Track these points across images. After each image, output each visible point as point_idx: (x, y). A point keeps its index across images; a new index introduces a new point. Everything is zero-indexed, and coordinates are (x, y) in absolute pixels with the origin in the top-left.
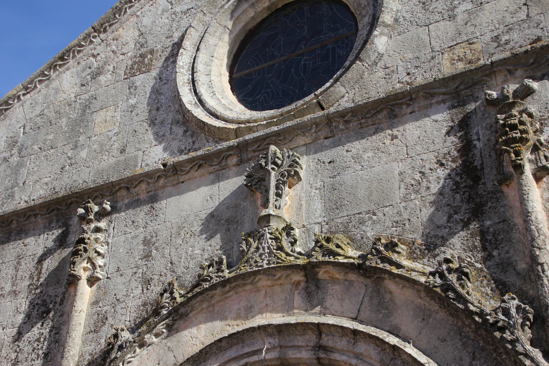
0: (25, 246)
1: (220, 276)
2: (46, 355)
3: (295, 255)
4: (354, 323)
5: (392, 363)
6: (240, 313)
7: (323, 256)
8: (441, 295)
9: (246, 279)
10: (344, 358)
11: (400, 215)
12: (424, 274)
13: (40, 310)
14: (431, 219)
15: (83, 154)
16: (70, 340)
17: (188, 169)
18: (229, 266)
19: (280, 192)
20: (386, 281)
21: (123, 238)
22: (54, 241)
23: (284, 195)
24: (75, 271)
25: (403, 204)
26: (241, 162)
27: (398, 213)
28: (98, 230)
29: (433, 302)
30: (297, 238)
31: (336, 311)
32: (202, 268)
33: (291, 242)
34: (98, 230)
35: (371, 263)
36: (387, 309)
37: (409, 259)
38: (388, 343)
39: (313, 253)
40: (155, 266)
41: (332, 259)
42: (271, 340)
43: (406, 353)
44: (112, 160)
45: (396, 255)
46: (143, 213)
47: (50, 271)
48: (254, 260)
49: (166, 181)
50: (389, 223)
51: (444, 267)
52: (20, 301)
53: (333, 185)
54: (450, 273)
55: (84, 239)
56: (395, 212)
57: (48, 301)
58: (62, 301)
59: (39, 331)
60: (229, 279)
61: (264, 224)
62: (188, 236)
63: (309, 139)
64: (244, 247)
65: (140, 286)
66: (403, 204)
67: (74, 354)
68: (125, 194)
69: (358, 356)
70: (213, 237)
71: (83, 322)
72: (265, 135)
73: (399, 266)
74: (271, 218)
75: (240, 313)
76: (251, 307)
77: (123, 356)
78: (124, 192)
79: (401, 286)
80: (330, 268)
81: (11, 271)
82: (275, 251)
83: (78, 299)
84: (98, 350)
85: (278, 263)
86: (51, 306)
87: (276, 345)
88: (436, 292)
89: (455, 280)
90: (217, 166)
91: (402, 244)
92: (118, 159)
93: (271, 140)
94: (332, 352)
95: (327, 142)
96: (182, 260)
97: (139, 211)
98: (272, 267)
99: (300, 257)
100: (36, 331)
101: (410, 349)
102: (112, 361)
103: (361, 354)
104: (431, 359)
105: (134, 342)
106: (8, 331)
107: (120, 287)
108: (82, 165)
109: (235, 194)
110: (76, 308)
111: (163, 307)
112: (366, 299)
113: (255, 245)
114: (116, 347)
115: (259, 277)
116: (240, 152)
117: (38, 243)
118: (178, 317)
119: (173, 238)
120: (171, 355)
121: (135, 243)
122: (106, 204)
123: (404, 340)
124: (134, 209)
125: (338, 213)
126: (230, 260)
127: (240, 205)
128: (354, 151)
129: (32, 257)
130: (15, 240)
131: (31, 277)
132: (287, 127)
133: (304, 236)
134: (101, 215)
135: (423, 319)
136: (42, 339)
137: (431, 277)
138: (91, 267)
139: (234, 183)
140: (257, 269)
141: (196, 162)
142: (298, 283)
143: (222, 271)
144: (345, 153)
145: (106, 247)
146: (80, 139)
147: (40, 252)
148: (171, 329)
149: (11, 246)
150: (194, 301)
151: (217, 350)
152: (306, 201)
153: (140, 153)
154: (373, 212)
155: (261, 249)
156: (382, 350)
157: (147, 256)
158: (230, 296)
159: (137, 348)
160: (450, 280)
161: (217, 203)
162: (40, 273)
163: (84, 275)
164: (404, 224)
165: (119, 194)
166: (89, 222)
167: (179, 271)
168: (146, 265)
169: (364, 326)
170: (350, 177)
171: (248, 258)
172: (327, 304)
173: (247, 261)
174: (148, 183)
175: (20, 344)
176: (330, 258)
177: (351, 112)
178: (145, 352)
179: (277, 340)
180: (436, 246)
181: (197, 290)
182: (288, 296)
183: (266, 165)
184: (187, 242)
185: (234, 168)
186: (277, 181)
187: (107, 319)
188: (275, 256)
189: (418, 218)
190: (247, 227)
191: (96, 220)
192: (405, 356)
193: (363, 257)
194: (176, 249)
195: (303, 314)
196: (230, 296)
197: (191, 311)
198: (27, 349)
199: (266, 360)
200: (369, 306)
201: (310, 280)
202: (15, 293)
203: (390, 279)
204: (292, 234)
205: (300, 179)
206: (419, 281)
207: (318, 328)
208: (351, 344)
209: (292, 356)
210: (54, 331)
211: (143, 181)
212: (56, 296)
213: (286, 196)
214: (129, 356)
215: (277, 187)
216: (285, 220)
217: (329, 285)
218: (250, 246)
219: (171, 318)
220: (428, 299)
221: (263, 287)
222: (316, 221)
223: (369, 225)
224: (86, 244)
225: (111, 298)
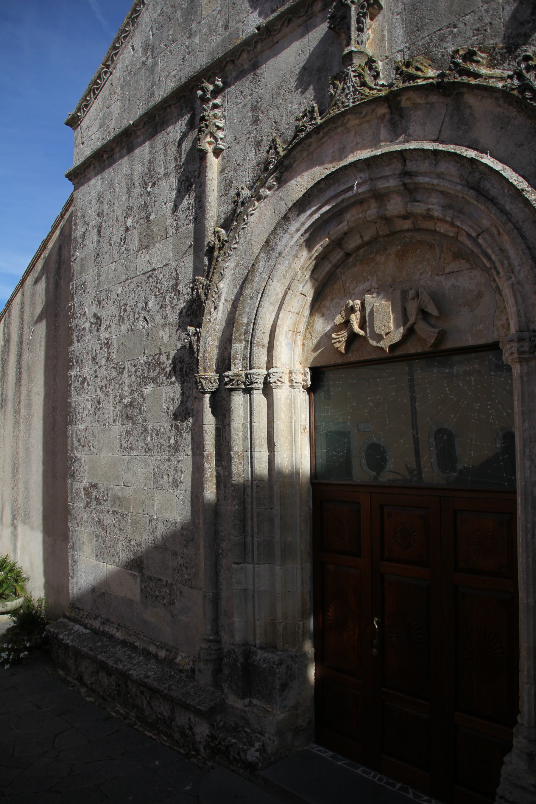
0: (168, 134)
2: (195, 219)
4: (434, 144)
5: (470, 176)
6: (335, 156)
7: (403, 83)
8: (518, 97)
10: (427, 180)
11: (481, 21)
12: (502, 79)
13: (186, 185)
14: (514, 16)
15: (197, 40)
16: (207, 205)
17: (279, 27)
18: (321, 114)
19: (362, 26)
20: (466, 96)
21: (235, 109)
22: (187, 125)
23: (365, 29)
24: (200, 146)
25: (485, 7)
27: (479, 19)
28: (215, 106)
29: (511, 108)
31: (419, 137)
32: (298, 120)
33: (373, 76)
34: (215, 106)
35: (449, 79)
36: (467, 125)
37: (490, 68)
38: (465, 157)
40: (263, 129)
41: (412, 84)
42: (362, 175)
43: (483, 163)
44: (219, 39)
45: (474, 65)
46: (248, 82)
47: (187, 151)
48: (341, 102)
49: (263, 45)
50: (470, 32)
51: (523, 66)
52: (171, 180)
54: (528, 71)
55: (204, 116)
56: (476, 18)
57: (190, 176)
58: (199, 174)
59: (188, 201)
60: (321, 124)
62: (286, 93)
65: (253, 149)
66: (485, 7)
67: (212, 215)
68: (231, 67)
69: (440, 176)
71: (215, 189)
73: (476, 76)
74: (353, 55)
75: (335, 156)
76: (344, 148)
77: (246, 210)
78: (230, 66)
79: (480, 98)
80: (411, 94)
81: (162, 158)
82: (358, 88)
83: (208, 170)
84: (229, 209)
85: (362, 99)
86: (192, 180)
87: (367, 179)
88: (514, 95)
89: (533, 78)
91: (482, 52)
92: (223, 36)
94: (417, 176)
96: (284, 118)
97: (245, 81)
99: (383, 88)
100: (185, 201)
101: (487, 160)
102: (238, 216)
103: (442, 173)
104: (508, 166)
105: (252, 197)
106: (168, 205)
107: (239, 153)
108: (197, 50)
109: (323, 41)
110: (207, 178)
111: (270, 163)
112: (447, 119)
113: (340, 86)
114: (239, 204)
115: (348, 117)
117: (176, 130)
118: (284, 169)
119: (275, 100)
120: (283, 203)
121: (245, 112)
122: (218, 81)
123: (482, 152)
124: (241, 80)
125: (419, 35)
129: (173, 142)
130: (161, 131)
131: (176, 160)
134: (217, 92)
135: (502, 128)
136: (191, 208)
137: (509, 81)
138: (213, 141)
139: (321, 30)
141: (285, 17)
142: (384, 116)
145: (224, 121)
146: (193, 26)
147: (179, 137)
148: (281, 181)
149: (159, 137)
150: (294, 153)
151: (318, 191)
152: (388, 30)
153: (241, 23)
154: (454, 25)
155: (347, 89)
156: (462, 166)
157: (256, 121)
158: (325, 142)
159: (256, 202)
160: (528, 79)
162: (181, 155)
163: (210, 149)
164: (486, 30)
165: (227, 69)
166: (208, 100)
167: (282, 128)
168: (256, 129)
169: (444, 146)
171: (336, 101)
172: (411, 131)
174: (249, 51)
175: (178, 214)
176: (410, 83)
178: (263, 204)
179: (367, 174)
180: (518, 46)
181: (296, 141)
182: (375, 131)
184: (286, 100)
186: (358, 14)
187: (232, 182)
188: (359, 92)
189: (500, 19)
191: (212, 98)
192: (481, 168)
193: (442, 75)
194: (278, 109)
195: (389, 146)
196: (325, 142)
197: (294, 162)
198: (183, 217)
199: (359, 194)
200: (450, 125)
202: (167, 175)
203: (469, 93)
204: (374, 67)
205: (380, 7)
206: (496, 87)
207: (402, 155)
208: (433, 166)
209: (381, 187)
210: (198, 200)
211: (243, 50)
212: (195, 171)
213: (368, 29)
214: (251, 209)
215: (359, 21)
217: (412, 112)
219: (278, 172)
220: (506, 106)
221: (353, 127)
222: (398, 49)
223: (450, 40)
224: (206, 120)
225: (233, 165)
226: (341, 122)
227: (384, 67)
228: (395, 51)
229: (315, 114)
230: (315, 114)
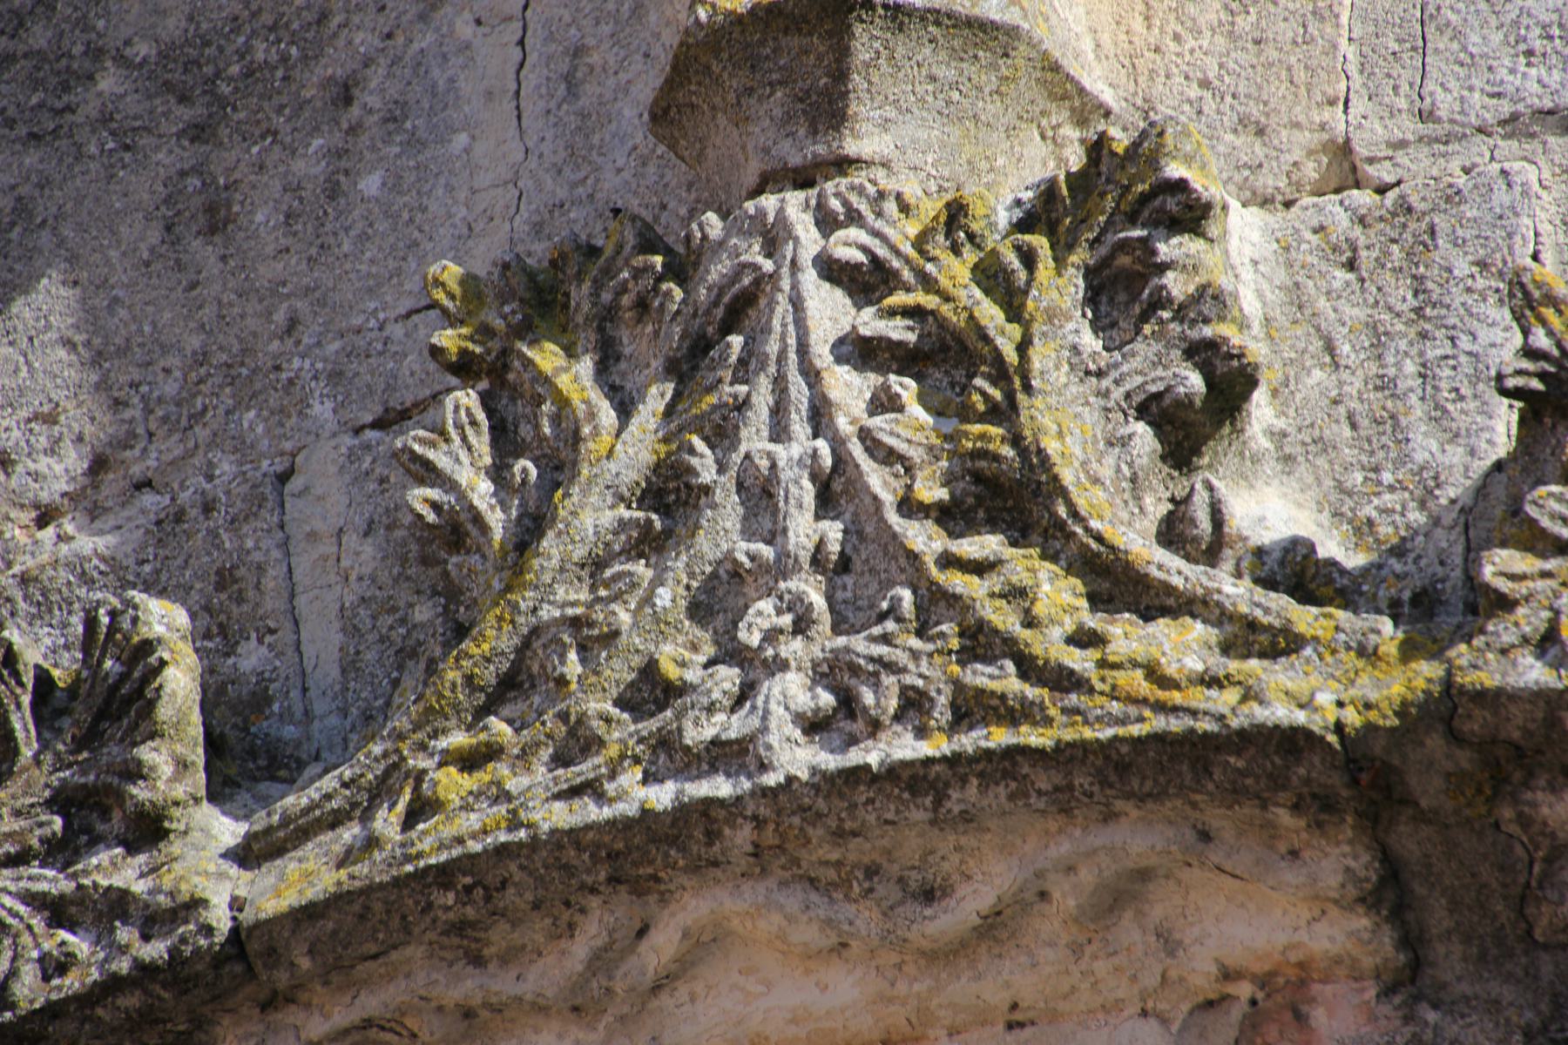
1: (118, 904)
3: (1235, 590)
9: (499, 937)
30: (1257, 349)
33: (1156, 409)
39: (1501, 565)
48: (619, 672)
60: (247, 946)
61: (767, 134)
64: (468, 469)
82: (924, 538)
85: (971, 708)
98: (894, 773)
99: (1305, 618)
113: (624, 447)
115: (693, 908)
126: (251, 657)
133: (1346, 313)
140: (662, 796)
143: (148, 831)
173: (512, 685)
188: (934, 601)
190: (491, 179)
201: (1450, 962)
204: (1177, 285)
216: (1058, 83)
218: (560, 467)
226: (580, 949)
227: (1296, 297)
228: (1482, 108)
229: (155, 756)
230: (155, 756)
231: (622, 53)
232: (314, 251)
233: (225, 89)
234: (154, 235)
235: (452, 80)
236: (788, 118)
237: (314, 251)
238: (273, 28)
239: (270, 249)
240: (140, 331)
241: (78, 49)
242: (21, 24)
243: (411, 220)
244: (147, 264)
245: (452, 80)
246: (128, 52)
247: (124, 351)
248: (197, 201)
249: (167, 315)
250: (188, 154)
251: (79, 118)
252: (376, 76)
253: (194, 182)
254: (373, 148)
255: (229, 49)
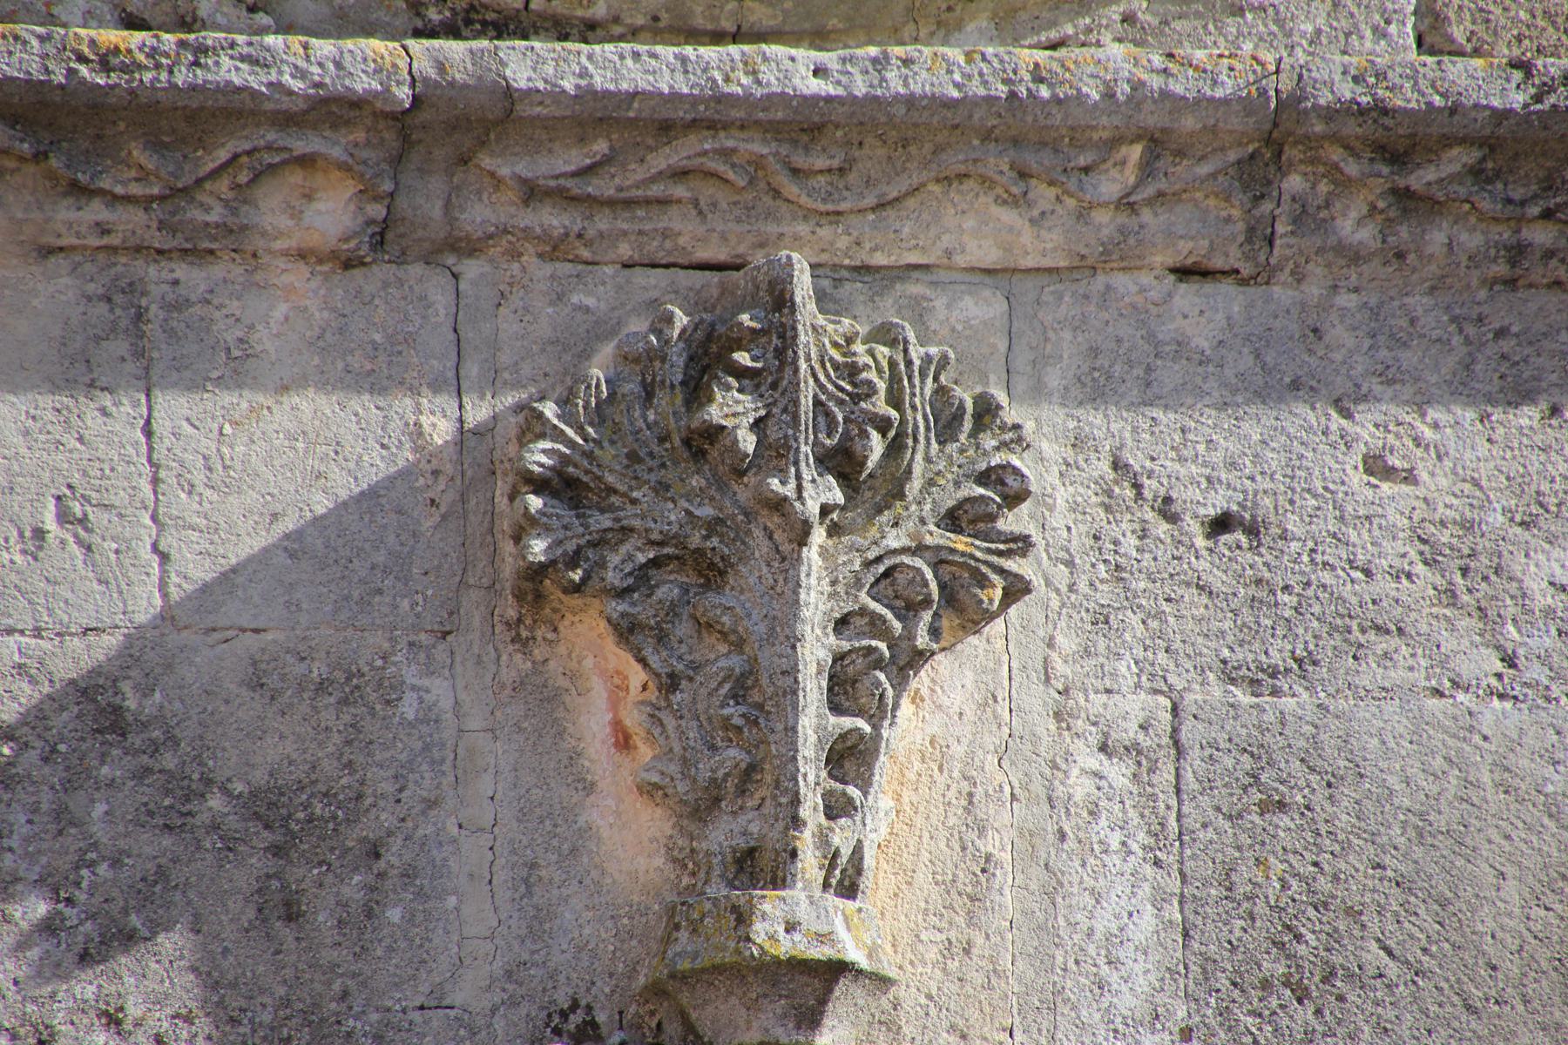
26: (379, 241)
53: (1258, 753)
63: (1053, 237)
70: (129, 939)
72: (694, 100)
90: (137, 216)
93: (726, 154)
95: (1199, 315)
109: (339, 551)
116: (397, 161)
127: (391, 692)
128: (1435, 480)
132: (910, 101)
144: (1357, 478)
161: (146, 604)
170: (1402, 725)
177: (1482, 142)
183: (775, 453)
185: (296, 276)
231: (564, 876)
232: (357, 949)
233: (294, 827)
234: (251, 913)
235: (445, 860)
236: (785, 1015)
237: (357, 949)
238: (326, 795)
239: (328, 941)
240: (244, 974)
241: (195, 776)
242: (157, 750)
243: (421, 946)
244: (247, 931)
245: (445, 860)
246: (229, 786)
247: (233, 985)
248: (278, 897)
249: (261, 968)
250: (272, 865)
251: (198, 821)
252: (396, 843)
253: (275, 884)
254: (395, 891)
255: (297, 801)
